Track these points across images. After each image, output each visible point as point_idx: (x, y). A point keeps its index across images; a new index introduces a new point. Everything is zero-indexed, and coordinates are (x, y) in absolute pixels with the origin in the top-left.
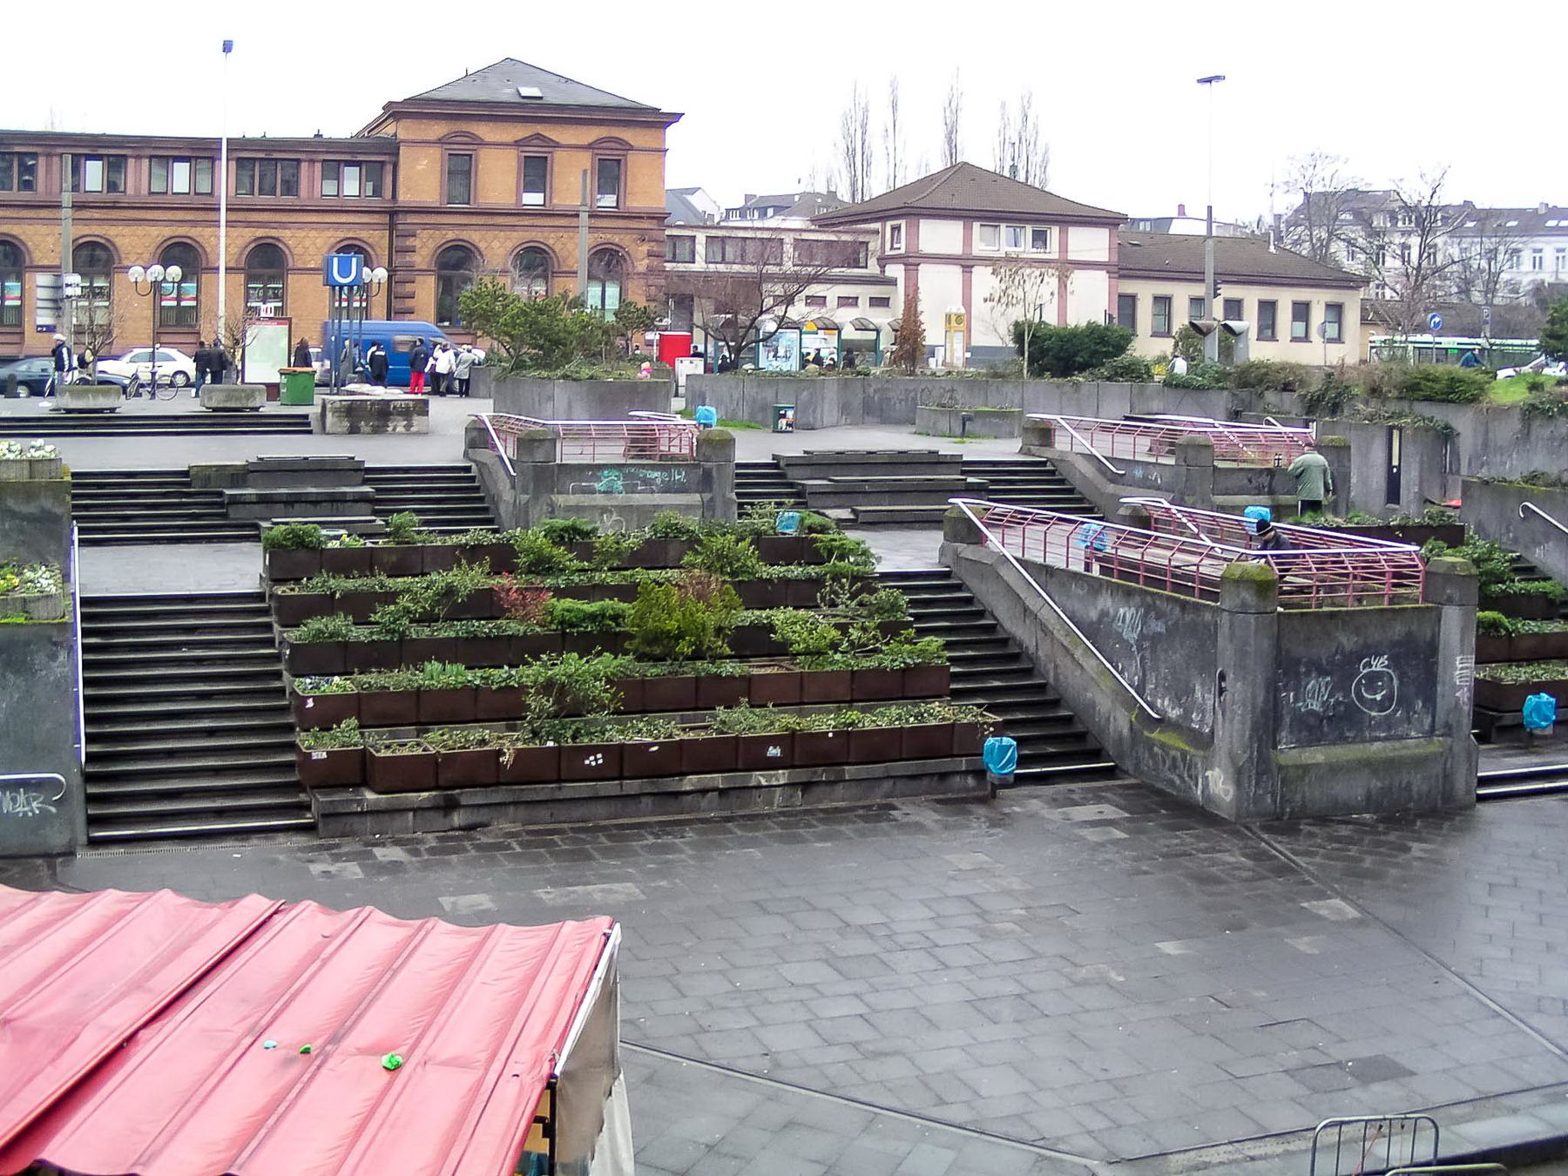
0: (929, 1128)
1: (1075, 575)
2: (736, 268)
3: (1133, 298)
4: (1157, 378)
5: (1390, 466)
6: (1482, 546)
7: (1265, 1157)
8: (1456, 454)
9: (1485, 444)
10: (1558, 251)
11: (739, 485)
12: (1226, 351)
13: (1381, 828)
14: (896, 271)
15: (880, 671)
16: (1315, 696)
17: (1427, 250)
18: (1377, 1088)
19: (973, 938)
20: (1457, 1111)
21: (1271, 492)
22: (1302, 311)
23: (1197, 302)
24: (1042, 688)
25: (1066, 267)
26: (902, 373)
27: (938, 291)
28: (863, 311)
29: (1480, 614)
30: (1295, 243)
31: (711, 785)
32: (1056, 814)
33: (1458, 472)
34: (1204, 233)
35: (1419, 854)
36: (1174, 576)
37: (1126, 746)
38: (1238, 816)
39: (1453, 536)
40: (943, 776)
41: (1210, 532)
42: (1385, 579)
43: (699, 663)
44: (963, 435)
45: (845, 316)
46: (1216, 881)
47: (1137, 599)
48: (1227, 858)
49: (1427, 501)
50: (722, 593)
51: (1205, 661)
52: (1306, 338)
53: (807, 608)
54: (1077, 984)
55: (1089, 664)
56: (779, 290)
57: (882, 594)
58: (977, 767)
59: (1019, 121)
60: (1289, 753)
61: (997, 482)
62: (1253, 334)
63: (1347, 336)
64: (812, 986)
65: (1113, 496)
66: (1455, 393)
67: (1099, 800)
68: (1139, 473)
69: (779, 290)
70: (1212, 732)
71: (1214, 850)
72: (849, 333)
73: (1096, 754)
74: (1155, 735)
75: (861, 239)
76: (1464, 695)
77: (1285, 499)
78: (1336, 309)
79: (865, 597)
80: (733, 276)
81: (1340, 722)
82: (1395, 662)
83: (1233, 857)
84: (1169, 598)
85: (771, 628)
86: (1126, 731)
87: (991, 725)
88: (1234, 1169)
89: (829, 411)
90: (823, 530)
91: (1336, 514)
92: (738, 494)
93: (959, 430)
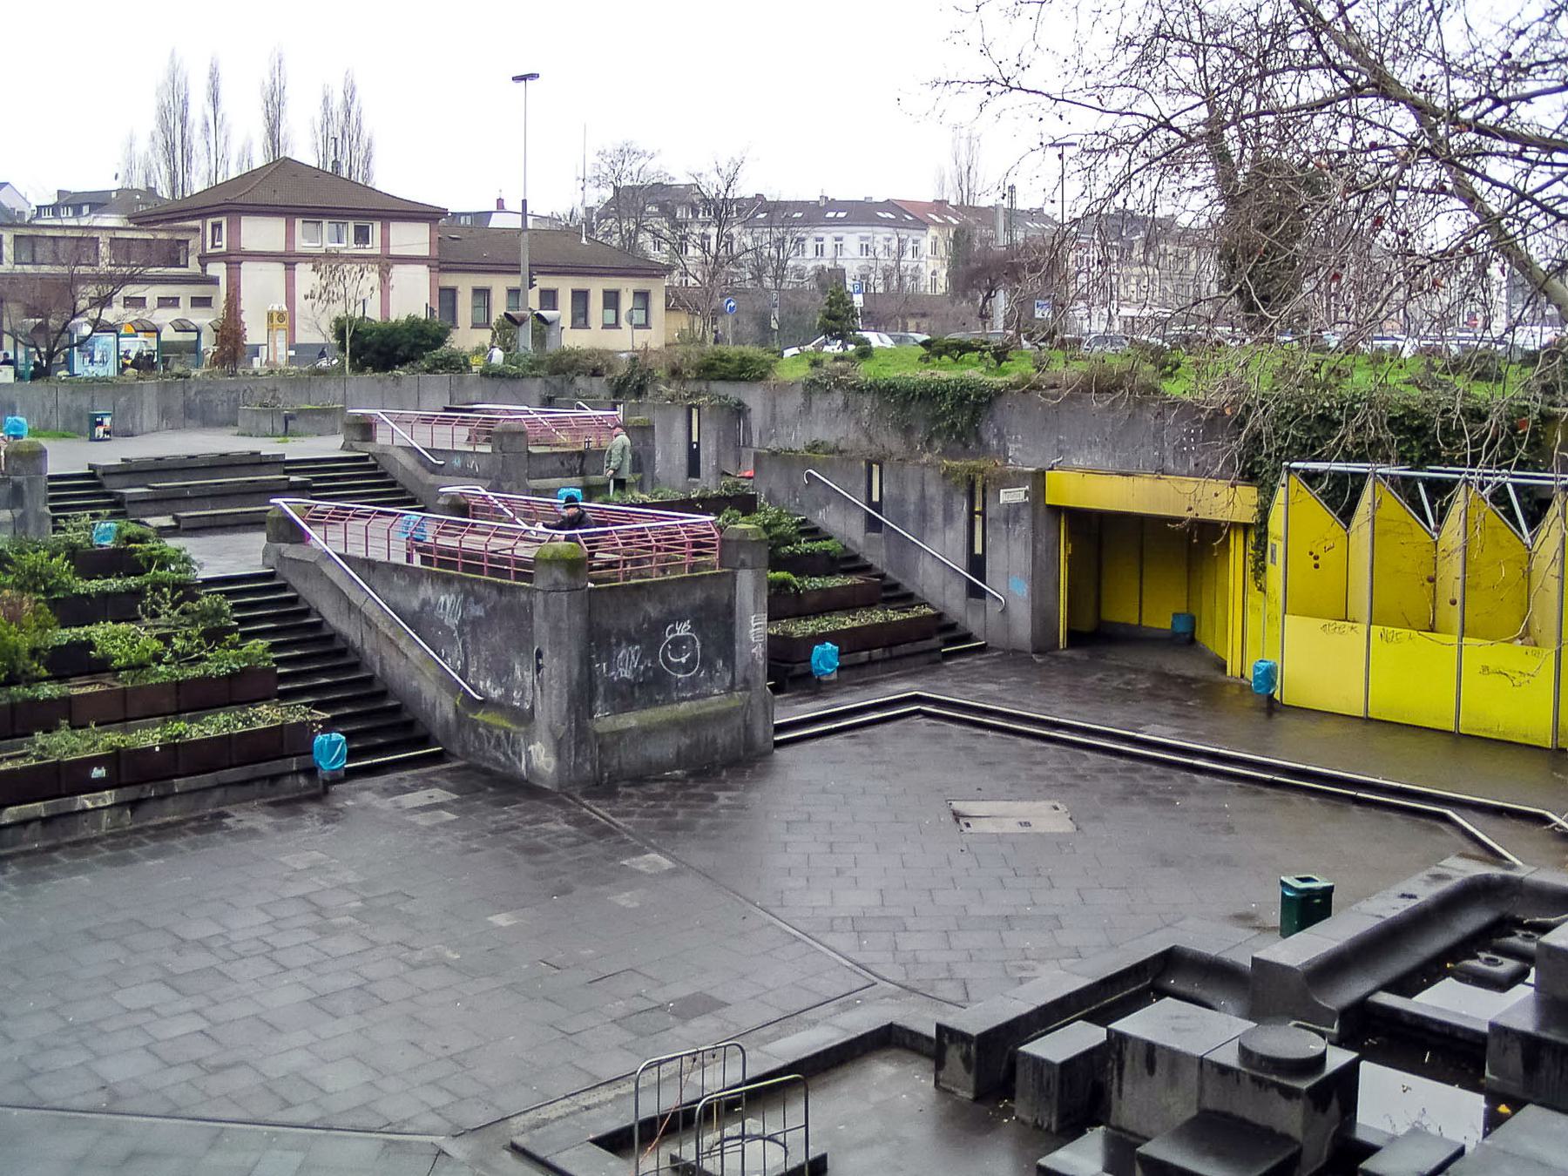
0: (276, 1134)
1: (397, 567)
2: (45, 269)
3: (453, 291)
4: (475, 369)
5: (690, 443)
6: (773, 511)
7: (599, 1105)
8: (748, 429)
9: (773, 418)
10: (837, 239)
11: (52, 499)
12: (540, 338)
13: (691, 781)
14: (217, 270)
15: (206, 679)
16: (626, 664)
17: (726, 240)
18: (696, 1023)
19: (310, 936)
20: (766, 1032)
21: (582, 474)
22: (611, 300)
23: (514, 293)
24: (369, 680)
25: (386, 262)
26: (223, 374)
27: (261, 288)
28: (183, 311)
29: (772, 575)
30: (606, 234)
31: (32, 815)
32: (387, 804)
33: (750, 445)
35: (727, 802)
36: (491, 560)
37: (453, 728)
38: (561, 787)
39: (746, 504)
40: (274, 779)
41: (527, 515)
42: (686, 549)
43: (14, 689)
44: (286, 433)
45: (164, 318)
46: (541, 850)
47: (457, 586)
48: (552, 826)
49: (725, 474)
50: (36, 612)
51: (522, 638)
52: (616, 325)
53: (128, 621)
54: (414, 968)
55: (414, 653)
56: (92, 291)
57: (206, 600)
58: (310, 765)
59: (342, 117)
60: (605, 720)
61: (319, 479)
62: (566, 321)
63: (653, 322)
64: (149, 1009)
65: (432, 486)
66: (746, 372)
67: (429, 784)
68: (457, 462)
69: (92, 291)
70: (532, 708)
71: (537, 821)
72: (169, 335)
73: (425, 741)
74: (479, 716)
75: (179, 237)
76: (759, 651)
77: (595, 479)
78: (643, 297)
79: (188, 605)
80: (42, 278)
81: (652, 686)
82: (696, 626)
83: (558, 825)
84: (486, 582)
85: (90, 645)
86: (451, 716)
87: (318, 722)
88: (571, 1121)
89: (148, 414)
90: (142, 539)
91: (642, 491)
92: (52, 508)
93: (281, 430)
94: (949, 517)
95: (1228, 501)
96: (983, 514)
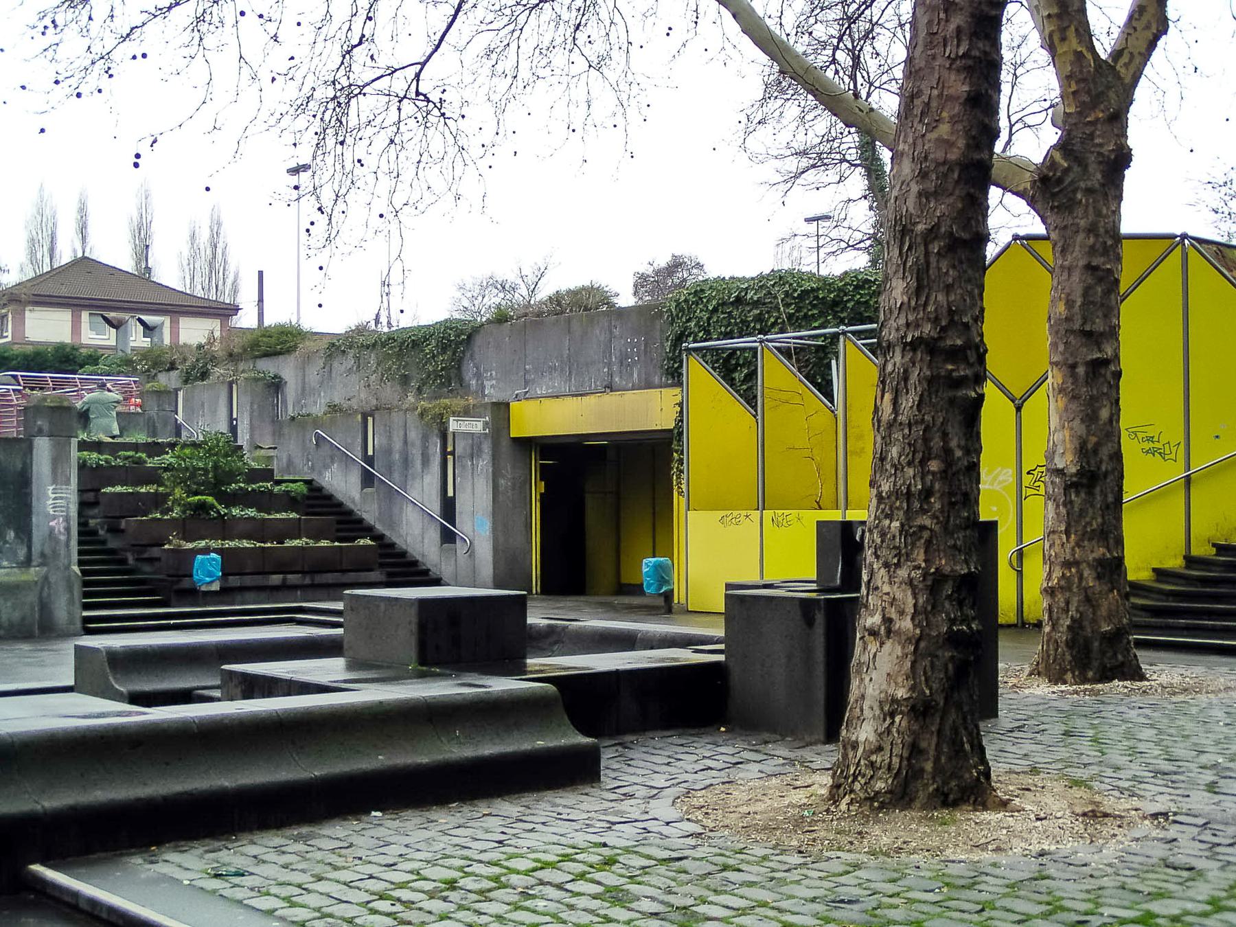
8: (285, 402)
34: (1001, 620)
59: (209, 252)
94: (426, 461)
95: (649, 409)
96: (453, 453)
